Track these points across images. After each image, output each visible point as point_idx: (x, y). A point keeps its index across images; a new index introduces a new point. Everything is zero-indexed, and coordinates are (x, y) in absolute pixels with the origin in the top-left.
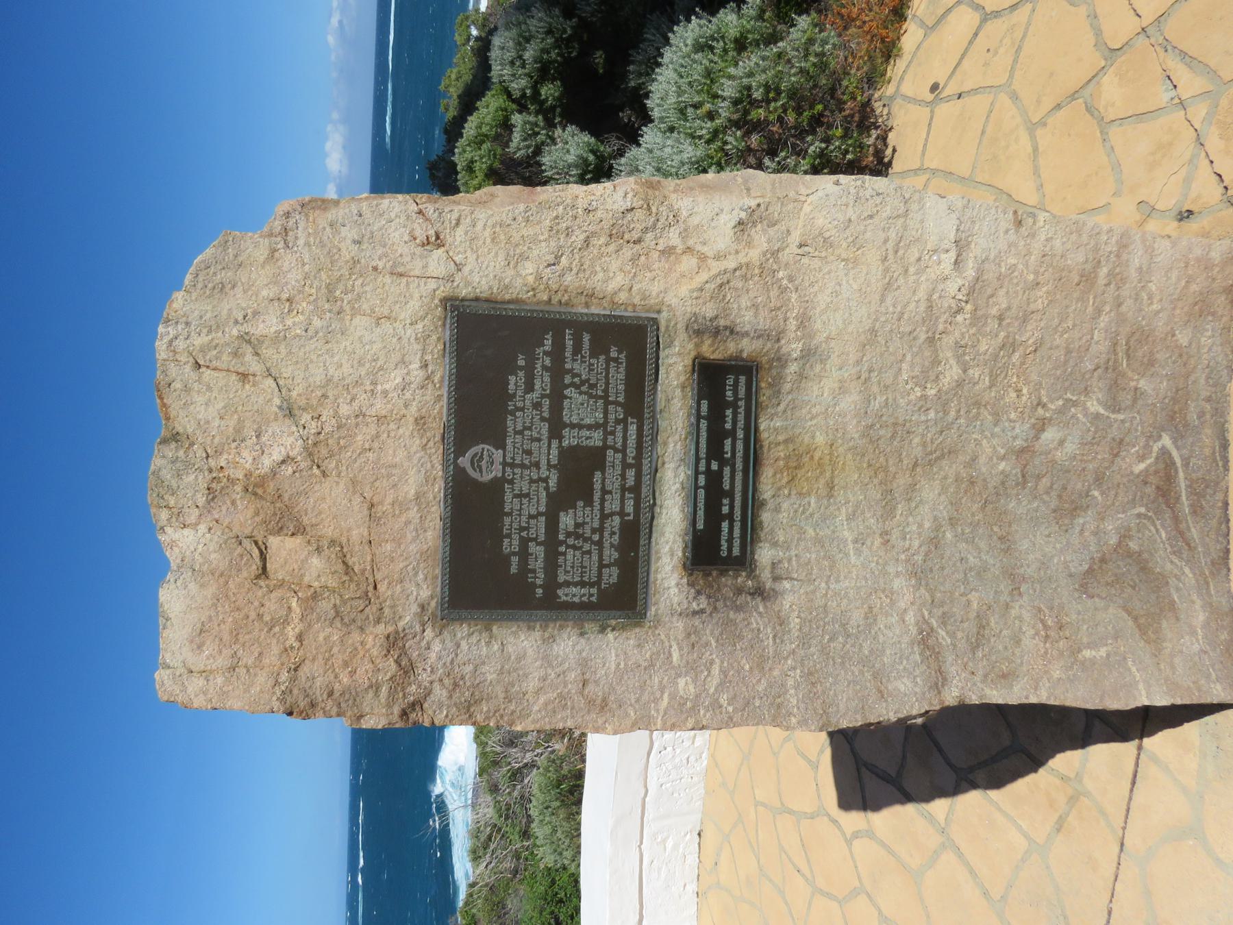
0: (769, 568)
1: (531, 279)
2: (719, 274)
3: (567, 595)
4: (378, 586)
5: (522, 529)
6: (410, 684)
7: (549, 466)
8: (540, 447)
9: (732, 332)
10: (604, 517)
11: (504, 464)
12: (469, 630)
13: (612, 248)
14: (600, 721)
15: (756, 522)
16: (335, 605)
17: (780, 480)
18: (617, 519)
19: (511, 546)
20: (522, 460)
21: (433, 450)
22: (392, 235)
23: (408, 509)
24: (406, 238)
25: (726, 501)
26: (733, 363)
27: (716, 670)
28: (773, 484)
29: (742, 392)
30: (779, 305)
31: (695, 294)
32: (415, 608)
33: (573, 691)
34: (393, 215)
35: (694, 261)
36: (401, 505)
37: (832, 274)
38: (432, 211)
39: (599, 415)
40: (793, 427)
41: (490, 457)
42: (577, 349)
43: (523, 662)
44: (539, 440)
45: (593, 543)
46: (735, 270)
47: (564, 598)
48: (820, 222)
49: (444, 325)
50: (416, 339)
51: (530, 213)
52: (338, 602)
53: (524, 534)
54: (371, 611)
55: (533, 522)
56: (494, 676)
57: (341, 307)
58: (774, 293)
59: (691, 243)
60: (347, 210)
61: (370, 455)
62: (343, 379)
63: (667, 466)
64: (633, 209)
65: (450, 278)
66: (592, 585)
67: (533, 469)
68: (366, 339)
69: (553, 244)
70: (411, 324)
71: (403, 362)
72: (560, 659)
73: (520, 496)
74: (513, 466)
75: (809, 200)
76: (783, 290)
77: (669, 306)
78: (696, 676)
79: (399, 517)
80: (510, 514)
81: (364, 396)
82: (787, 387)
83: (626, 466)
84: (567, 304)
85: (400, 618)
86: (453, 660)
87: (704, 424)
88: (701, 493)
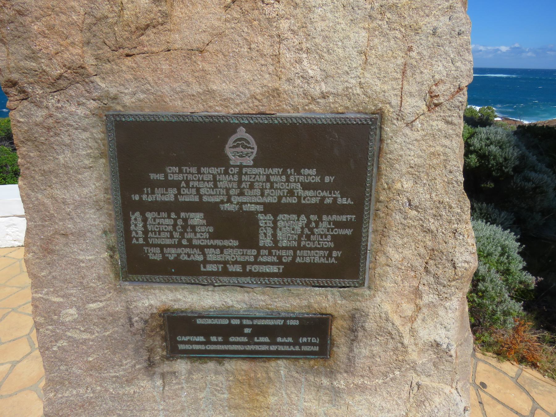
0: (171, 370)
1: (398, 186)
2: (399, 332)
3: (135, 219)
4: (129, 58)
5: (187, 182)
6: (42, 88)
7: (241, 204)
8: (256, 196)
9: (353, 340)
10: (202, 248)
11: (241, 167)
12: (99, 139)
13: (422, 251)
14: (34, 248)
15: (206, 359)
16: (107, 17)
17: (239, 374)
18: (200, 258)
19: (173, 173)
20: (244, 181)
21: (251, 105)
22: (440, 64)
23: (200, 84)
24: (437, 77)
25: (220, 339)
26: (329, 342)
27: (85, 336)
28: (237, 370)
29: (305, 348)
30: (374, 372)
31: (383, 315)
32: (113, 91)
33: (57, 227)
34: (459, 64)
35: (409, 313)
36: (202, 77)
37: (396, 406)
38: (461, 99)
39: (284, 243)
40: (280, 382)
41: (247, 154)
42: (339, 225)
43: (77, 185)
44: (262, 195)
45: (180, 241)
46: (402, 344)
47: (133, 218)
48: (437, 399)
49: (359, 112)
50: (347, 88)
51: (456, 185)
52: (111, 20)
53: (183, 184)
54: (106, 52)
55: (194, 191)
56: (63, 161)
57: (376, 19)
58: (383, 369)
59: (425, 310)
60: (464, 21)
61: (245, 49)
62: (312, 23)
63: (246, 295)
64: (455, 268)
65: (400, 116)
66: (146, 239)
67: (238, 191)
68: (347, 42)
69: (428, 204)
70: (360, 83)
71: (327, 77)
72: (82, 215)
73: (215, 181)
74: (240, 174)
75: (454, 391)
76: (385, 375)
77: (375, 296)
78: (79, 322)
79: (193, 76)
80: (199, 172)
81: (297, 42)
82: (312, 378)
83: (244, 264)
84: (376, 215)
85: (103, 78)
86: (72, 126)
87: (280, 322)
88: (226, 322)
